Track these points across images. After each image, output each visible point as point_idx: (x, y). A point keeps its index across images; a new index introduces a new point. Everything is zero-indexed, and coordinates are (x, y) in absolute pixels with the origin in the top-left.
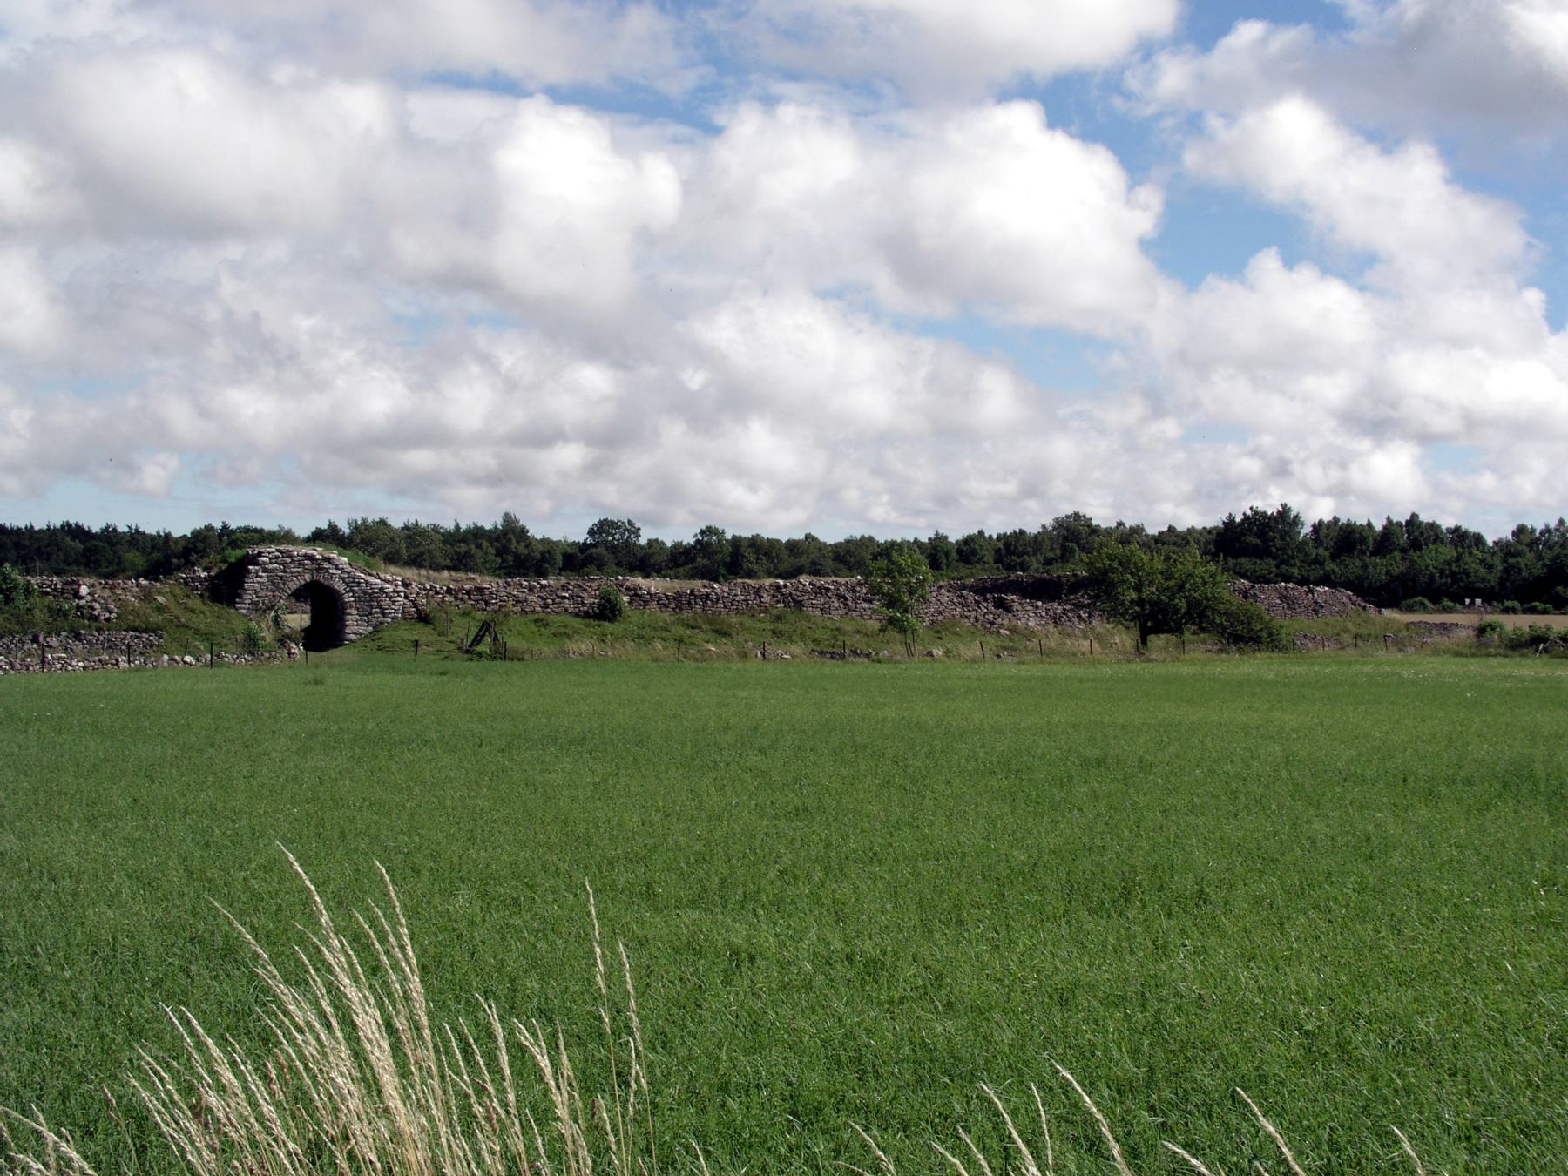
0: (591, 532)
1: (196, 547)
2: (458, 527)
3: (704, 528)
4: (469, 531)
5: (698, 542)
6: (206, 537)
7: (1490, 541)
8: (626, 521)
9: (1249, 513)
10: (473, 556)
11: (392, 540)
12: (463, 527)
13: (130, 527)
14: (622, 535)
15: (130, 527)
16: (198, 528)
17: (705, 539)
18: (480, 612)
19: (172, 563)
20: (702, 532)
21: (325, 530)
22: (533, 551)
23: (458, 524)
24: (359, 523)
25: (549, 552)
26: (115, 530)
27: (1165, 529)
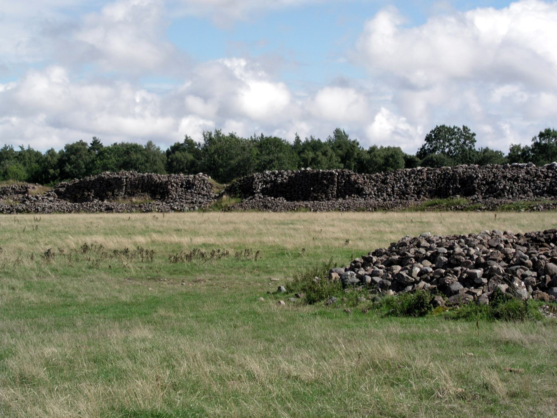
0: (428, 139)
1: (69, 158)
2: (298, 140)
3: (543, 131)
4: (307, 143)
5: (536, 144)
6: (77, 150)
7: (348, 139)
8: (462, 128)
9: (310, 140)
10: (319, 162)
11: (244, 149)
12: (303, 140)
13: (22, 148)
14: (458, 140)
15: (22, 148)
16: (138, 144)
17: (543, 142)
18: (335, 217)
19: (49, 173)
20: (541, 135)
21: (182, 144)
22: (375, 156)
23: (298, 138)
24: (213, 136)
25: (392, 156)
26: (12, 150)
27: (51, 149)
